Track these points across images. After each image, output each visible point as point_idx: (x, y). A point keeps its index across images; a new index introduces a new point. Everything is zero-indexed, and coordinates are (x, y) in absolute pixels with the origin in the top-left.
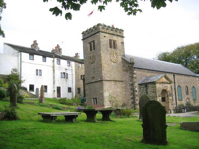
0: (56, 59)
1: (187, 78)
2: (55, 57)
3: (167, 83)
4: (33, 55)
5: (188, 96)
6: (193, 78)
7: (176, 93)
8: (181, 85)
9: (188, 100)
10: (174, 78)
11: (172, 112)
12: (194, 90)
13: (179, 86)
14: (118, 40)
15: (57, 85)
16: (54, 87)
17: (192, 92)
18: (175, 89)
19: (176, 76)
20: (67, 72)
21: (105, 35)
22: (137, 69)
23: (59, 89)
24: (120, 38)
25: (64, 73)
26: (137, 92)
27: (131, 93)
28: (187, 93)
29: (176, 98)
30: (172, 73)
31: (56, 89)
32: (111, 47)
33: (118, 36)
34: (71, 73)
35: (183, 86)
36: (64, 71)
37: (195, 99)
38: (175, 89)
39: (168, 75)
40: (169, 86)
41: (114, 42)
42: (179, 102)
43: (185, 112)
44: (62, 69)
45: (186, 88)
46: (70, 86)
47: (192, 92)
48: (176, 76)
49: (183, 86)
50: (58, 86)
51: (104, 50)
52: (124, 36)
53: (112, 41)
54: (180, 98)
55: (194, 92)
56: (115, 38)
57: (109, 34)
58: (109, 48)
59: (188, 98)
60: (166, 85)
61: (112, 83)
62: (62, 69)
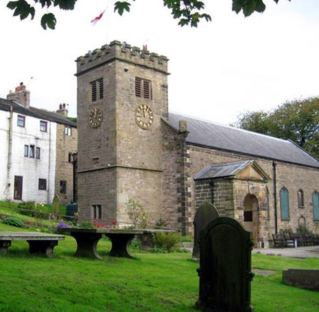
0: (15, 115)
3: (258, 181)
5: (303, 212)
9: (302, 221)
10: (274, 170)
11: (267, 244)
13: (284, 189)
14: (155, 80)
15: (15, 172)
17: (311, 204)
18: (275, 194)
21: (128, 66)
23: (18, 181)
24: (159, 76)
25: (32, 147)
26: (190, 196)
27: (178, 199)
29: (276, 215)
31: (12, 182)
32: (138, 95)
33: (155, 70)
36: (33, 142)
38: (275, 194)
40: (261, 187)
41: (147, 83)
43: (294, 247)
44: (28, 136)
45: (300, 193)
49: (293, 188)
50: (18, 175)
51: (122, 100)
53: (142, 81)
54: (285, 215)
56: (148, 75)
57: (135, 65)
58: (134, 97)
59: (302, 217)
60: (255, 184)
61: (138, 175)
62: (28, 136)
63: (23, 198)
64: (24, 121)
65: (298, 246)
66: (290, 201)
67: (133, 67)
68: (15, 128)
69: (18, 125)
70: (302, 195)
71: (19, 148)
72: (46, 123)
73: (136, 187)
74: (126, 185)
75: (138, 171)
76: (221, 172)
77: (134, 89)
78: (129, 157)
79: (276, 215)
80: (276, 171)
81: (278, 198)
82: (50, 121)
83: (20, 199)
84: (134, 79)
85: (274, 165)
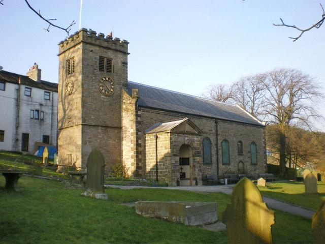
0: (23, 87)
1: (241, 127)
2: (22, 84)
3: (193, 134)
4: (5, 83)
5: (241, 158)
6: (254, 128)
7: (217, 152)
8: (230, 139)
9: (241, 165)
10: (217, 126)
11: (200, 182)
12: (253, 147)
13: (225, 140)
14: (117, 60)
15: (23, 130)
16: (17, 134)
17: (249, 152)
18: (217, 145)
19: (221, 124)
20: (43, 109)
21: (93, 48)
22: (144, 109)
23: (26, 137)
24: (120, 55)
25: (38, 111)
26: (141, 147)
27: (132, 148)
28: (240, 152)
29: (217, 160)
30: (212, 118)
31: (20, 137)
32: (101, 69)
33: (116, 50)
34: (50, 111)
35: (233, 141)
36: (38, 107)
37: (254, 161)
38: (217, 145)
39: (196, 122)
40: (196, 139)
41: (109, 61)
42: (224, 167)
43: (224, 184)
44: (34, 103)
45: (239, 144)
46: (48, 133)
47: (249, 152)
48: (221, 124)
49: (233, 141)
50: (25, 132)
51: (87, 73)
52: (128, 52)
53: (105, 60)
54: (226, 160)
55: (254, 151)
56: (110, 54)
57: (100, 46)
58: (97, 72)
59: (241, 161)
60: (191, 137)
61: (100, 131)
62: (34, 103)
63: (29, 150)
64: (31, 92)
65: (228, 184)
66: (231, 150)
67: (98, 48)
68: (23, 97)
69: (25, 95)
70: (242, 145)
71: (26, 111)
72: (49, 93)
73: (98, 140)
74: (89, 138)
75: (100, 127)
76: (164, 128)
77: (98, 65)
78: (92, 117)
79: (217, 160)
80: (218, 128)
81: (220, 147)
82: (53, 91)
83: (27, 150)
84: (98, 57)
85: (216, 123)
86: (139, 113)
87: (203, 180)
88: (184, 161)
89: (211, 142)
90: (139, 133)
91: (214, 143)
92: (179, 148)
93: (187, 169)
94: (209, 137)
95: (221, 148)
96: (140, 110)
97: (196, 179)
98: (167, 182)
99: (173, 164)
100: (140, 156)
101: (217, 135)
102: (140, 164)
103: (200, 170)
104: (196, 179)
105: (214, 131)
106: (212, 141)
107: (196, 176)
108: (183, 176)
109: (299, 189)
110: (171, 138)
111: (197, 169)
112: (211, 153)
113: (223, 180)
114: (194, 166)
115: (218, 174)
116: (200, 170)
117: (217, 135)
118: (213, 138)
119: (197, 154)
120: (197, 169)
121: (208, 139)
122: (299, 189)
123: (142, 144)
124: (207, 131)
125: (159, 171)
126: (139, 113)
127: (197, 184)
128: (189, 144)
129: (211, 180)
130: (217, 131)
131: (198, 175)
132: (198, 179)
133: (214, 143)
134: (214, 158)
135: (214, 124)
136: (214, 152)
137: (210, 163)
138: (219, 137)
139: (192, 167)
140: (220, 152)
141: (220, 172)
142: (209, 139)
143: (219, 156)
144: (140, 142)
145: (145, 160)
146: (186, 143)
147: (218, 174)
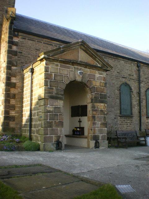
11: (104, 144)
18: (139, 94)
19: (144, 69)
29: (140, 112)
38: (139, 94)
60: (88, 71)
79: (140, 112)
80: (141, 73)
81: (143, 97)
85: (138, 67)
86: (15, 40)
87: (109, 139)
88: (79, 111)
89: (131, 89)
90: (13, 68)
91: (135, 91)
92: (64, 87)
93: (86, 122)
94: (128, 82)
95: (144, 97)
96: (17, 36)
97: (96, 138)
98: (40, 142)
99: (49, 112)
100: (13, 102)
101: (139, 82)
102: (13, 113)
103: (105, 124)
104: (96, 138)
105: (135, 76)
106: (133, 88)
107: (97, 133)
108: (78, 133)
109: (38, 60)
110: (46, 70)
111: (98, 123)
112: (131, 103)
113: (143, 139)
114: (94, 117)
115: (140, 129)
116: (105, 124)
117: (139, 82)
118: (134, 86)
119: (102, 98)
120: (98, 123)
121: (126, 84)
122: (38, 60)
123: (18, 84)
124: (126, 75)
125: (33, 123)
126: (15, 40)
127: (97, 146)
128: (85, 81)
129: (123, 140)
130: (139, 76)
131: (101, 131)
132: (100, 138)
133: (135, 91)
134: (135, 110)
135: (135, 68)
136: (135, 102)
137: (130, 116)
138: (142, 85)
139: (91, 119)
140: (144, 103)
141: (143, 128)
142: (129, 85)
143: (142, 108)
144: (13, 80)
145: (22, 107)
146: (79, 79)
147: (140, 129)
